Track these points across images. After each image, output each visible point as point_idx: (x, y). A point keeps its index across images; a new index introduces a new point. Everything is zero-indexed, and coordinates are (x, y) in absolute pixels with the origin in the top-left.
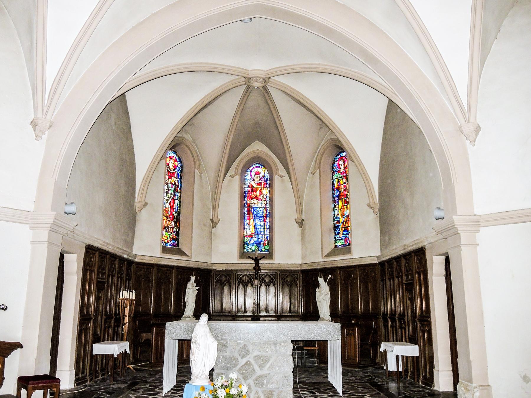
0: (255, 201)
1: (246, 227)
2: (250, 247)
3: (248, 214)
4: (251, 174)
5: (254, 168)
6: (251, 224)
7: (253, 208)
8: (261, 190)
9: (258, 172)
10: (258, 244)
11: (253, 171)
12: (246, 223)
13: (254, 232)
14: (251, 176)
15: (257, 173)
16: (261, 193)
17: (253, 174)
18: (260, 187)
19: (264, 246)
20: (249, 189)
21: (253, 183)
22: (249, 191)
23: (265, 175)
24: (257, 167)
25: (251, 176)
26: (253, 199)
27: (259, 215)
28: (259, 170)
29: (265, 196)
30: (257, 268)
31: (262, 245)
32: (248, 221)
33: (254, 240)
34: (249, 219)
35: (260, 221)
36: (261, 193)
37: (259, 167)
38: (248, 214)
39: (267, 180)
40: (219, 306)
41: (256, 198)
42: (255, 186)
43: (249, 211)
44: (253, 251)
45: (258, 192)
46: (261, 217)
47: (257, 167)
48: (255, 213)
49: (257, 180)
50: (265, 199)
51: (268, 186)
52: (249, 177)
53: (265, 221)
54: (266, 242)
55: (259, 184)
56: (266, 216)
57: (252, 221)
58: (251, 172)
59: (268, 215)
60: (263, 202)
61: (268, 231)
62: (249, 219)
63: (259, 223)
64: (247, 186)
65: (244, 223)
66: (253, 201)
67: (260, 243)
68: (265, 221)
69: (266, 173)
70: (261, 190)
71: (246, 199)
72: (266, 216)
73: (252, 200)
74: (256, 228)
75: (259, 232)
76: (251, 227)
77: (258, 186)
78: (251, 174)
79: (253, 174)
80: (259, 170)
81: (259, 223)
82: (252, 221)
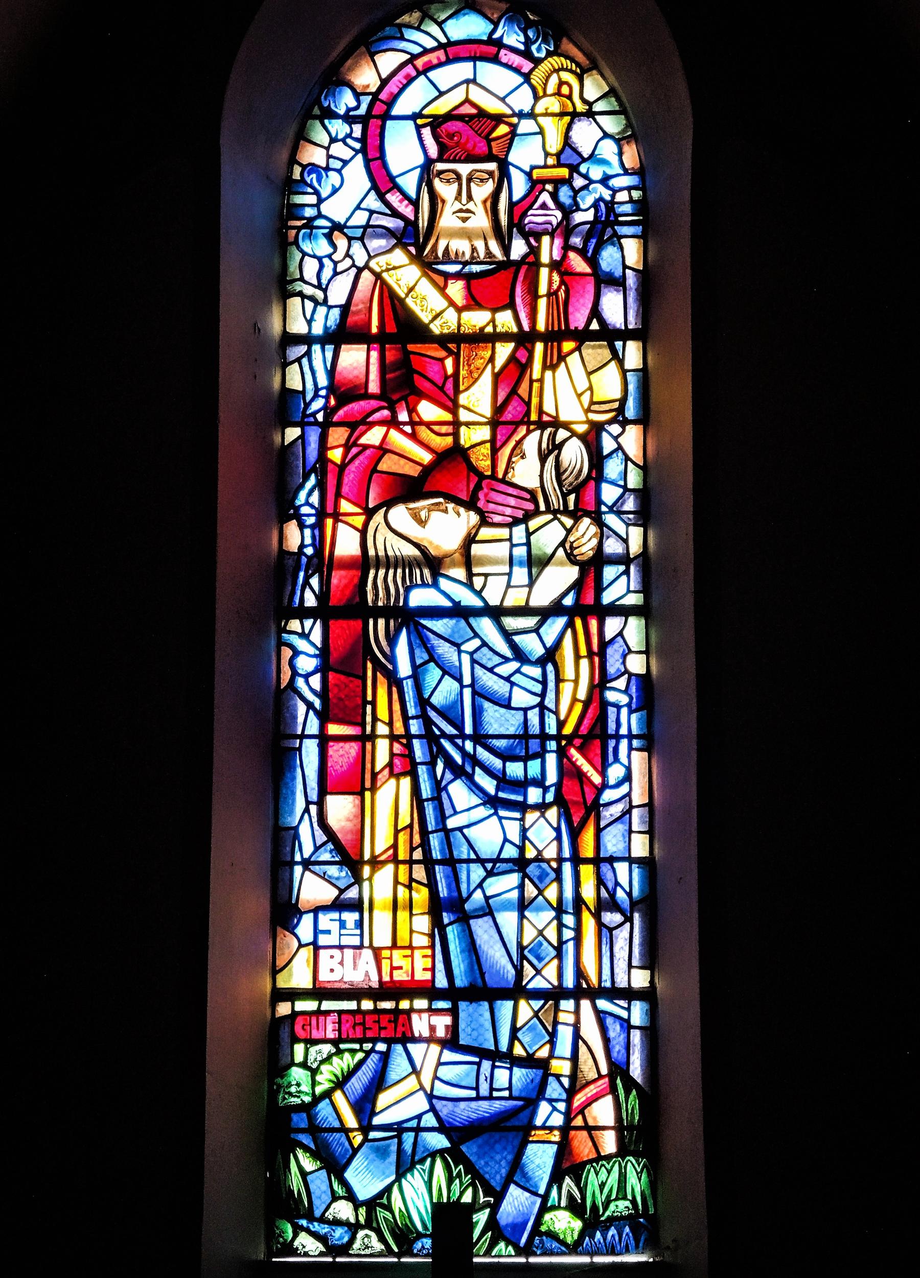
0: (445, 527)
1: (312, 889)
2: (365, 1178)
3: (343, 703)
4: (373, 154)
5: (417, 67)
6: (381, 839)
7: (408, 618)
8: (518, 368)
9: (484, 120)
10: (485, 1140)
11: (413, 99)
12: (308, 838)
13: (418, 966)
14: (382, 181)
15: (469, 136)
16: (514, 414)
17: (404, 150)
18: (505, 321)
19: (567, 1166)
20: (353, 358)
21: (404, 274)
22: (343, 391)
23: (569, 157)
24: (454, 51)
25: (382, 181)
26: (408, 489)
27: (497, 721)
28: (495, 87)
29: (574, 454)
30: (360, 1024)
31: (540, 1158)
32: (340, 809)
33: (422, 1081)
34: (358, 782)
35: (506, 798)
36: (514, 414)
37: (487, 51)
38: (343, 703)
39: (604, 229)
40: (320, 1021)
41: (451, 476)
42: (434, 305)
43: (348, 665)
44: (404, 1236)
45: (478, 398)
46: (527, 744)
47: (454, 51)
48: (444, 692)
49: (464, 223)
50: (581, 499)
51: (614, 308)
52: (346, 194)
53: (579, 806)
54: (603, 1112)
55: (492, 284)
56: (595, 735)
57: (391, 800)
58: (375, 117)
59: (630, 722)
60: (548, 535)
61: (627, 940)
62: (358, 782)
63: (489, 834)
64: (324, 321)
65: (282, 839)
66: (406, 528)
67: (512, 1126)
68: (579, 806)
69: (585, 135)
70: (518, 368)
71: (307, 498)
72: (595, 735)
73: (400, 515)
74: (450, 910)
75: (498, 960)
76: (381, 885)
77: (477, 319)
78: (373, 154)
79: (404, 150)
80: (495, 87)
81: (489, 834)
82: (391, 800)
